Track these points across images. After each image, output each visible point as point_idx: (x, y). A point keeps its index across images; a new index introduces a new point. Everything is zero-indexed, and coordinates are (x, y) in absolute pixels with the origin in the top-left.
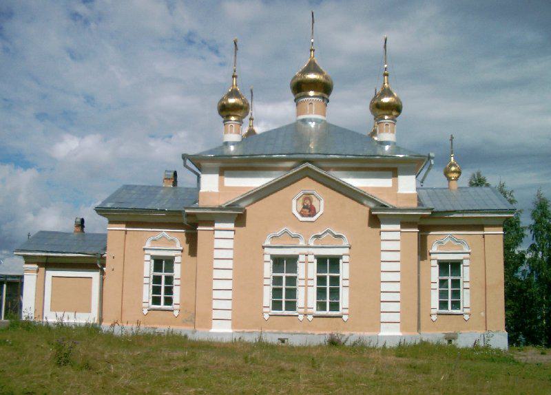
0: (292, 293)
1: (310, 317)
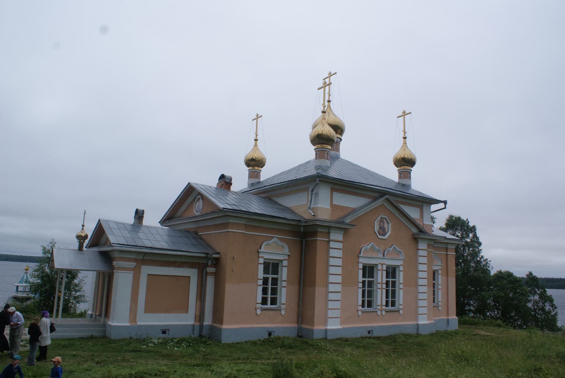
1: (384, 313)
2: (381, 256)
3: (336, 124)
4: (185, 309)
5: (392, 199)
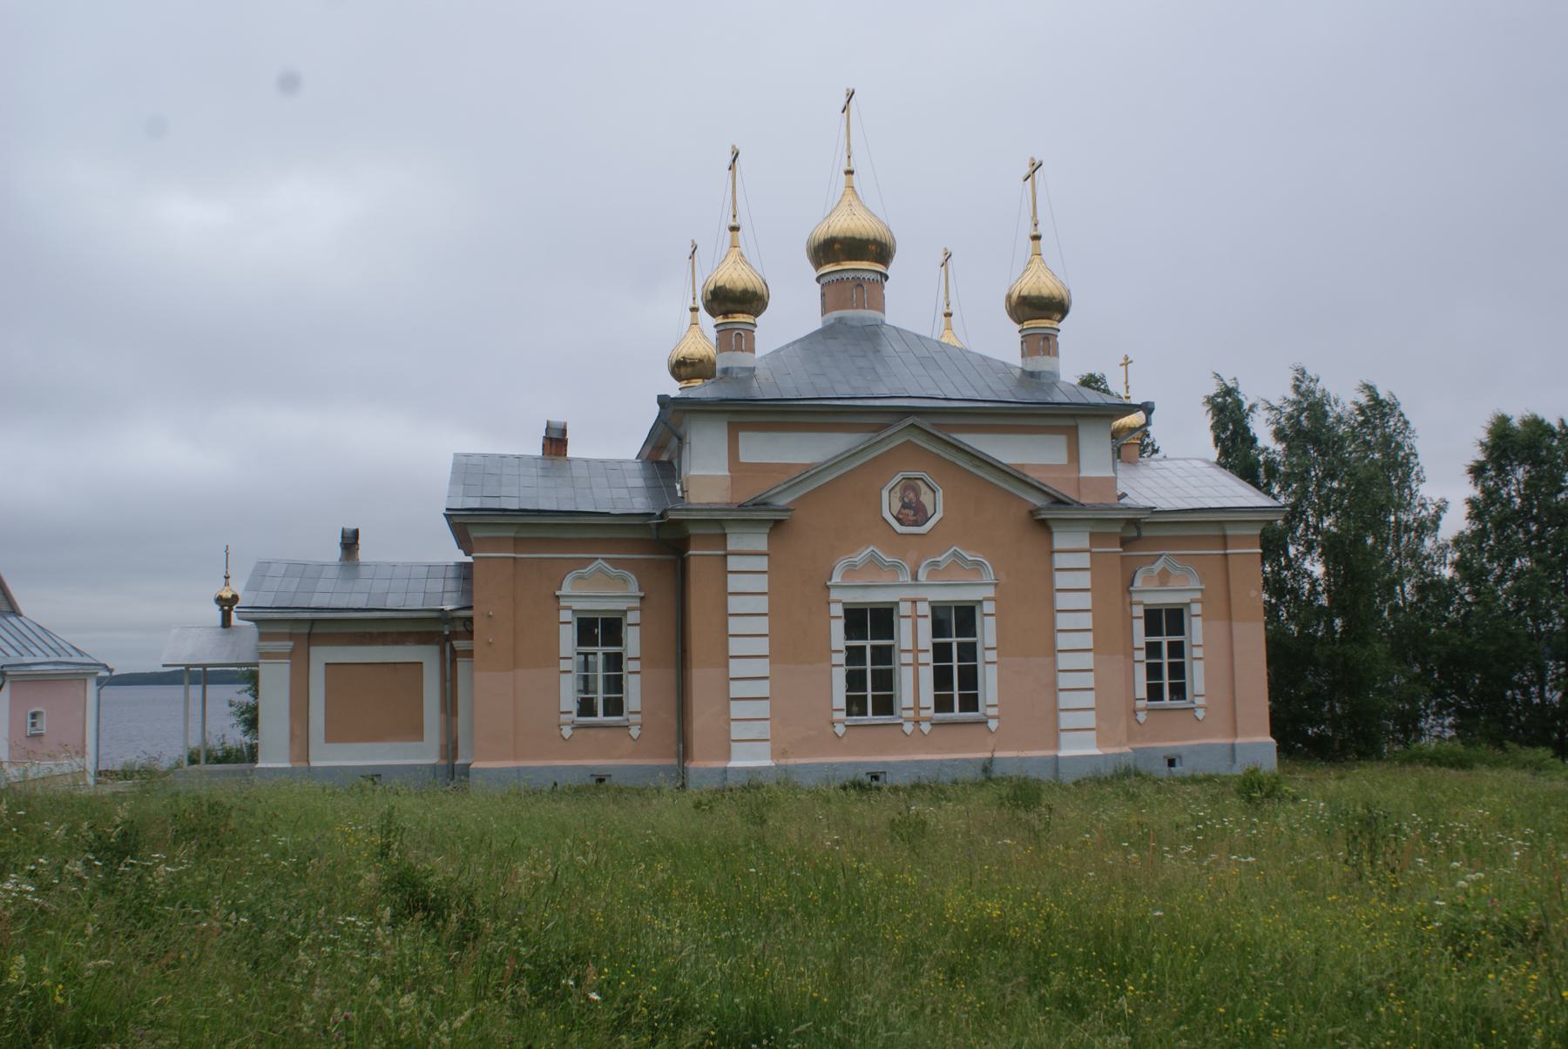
0: (885, 680)
1: (926, 727)
2: (906, 578)
3: (849, 234)
4: (415, 731)
5: (924, 423)
